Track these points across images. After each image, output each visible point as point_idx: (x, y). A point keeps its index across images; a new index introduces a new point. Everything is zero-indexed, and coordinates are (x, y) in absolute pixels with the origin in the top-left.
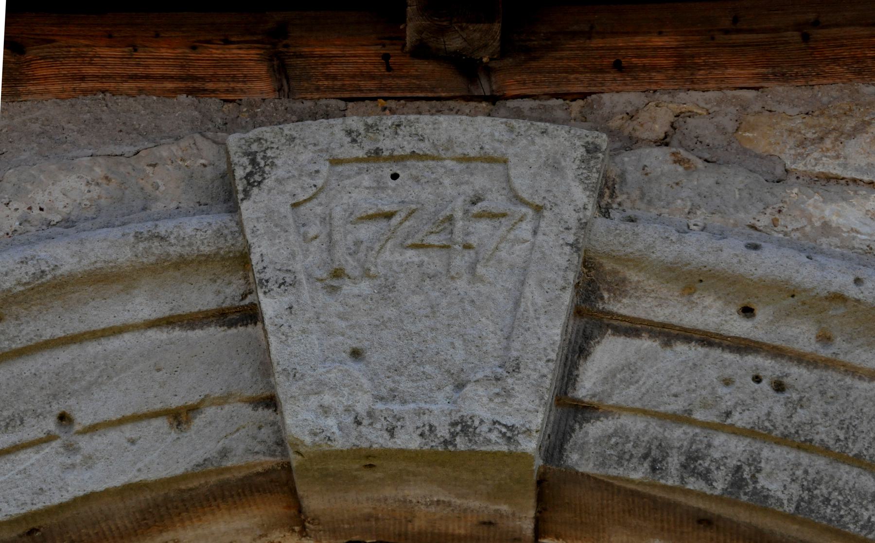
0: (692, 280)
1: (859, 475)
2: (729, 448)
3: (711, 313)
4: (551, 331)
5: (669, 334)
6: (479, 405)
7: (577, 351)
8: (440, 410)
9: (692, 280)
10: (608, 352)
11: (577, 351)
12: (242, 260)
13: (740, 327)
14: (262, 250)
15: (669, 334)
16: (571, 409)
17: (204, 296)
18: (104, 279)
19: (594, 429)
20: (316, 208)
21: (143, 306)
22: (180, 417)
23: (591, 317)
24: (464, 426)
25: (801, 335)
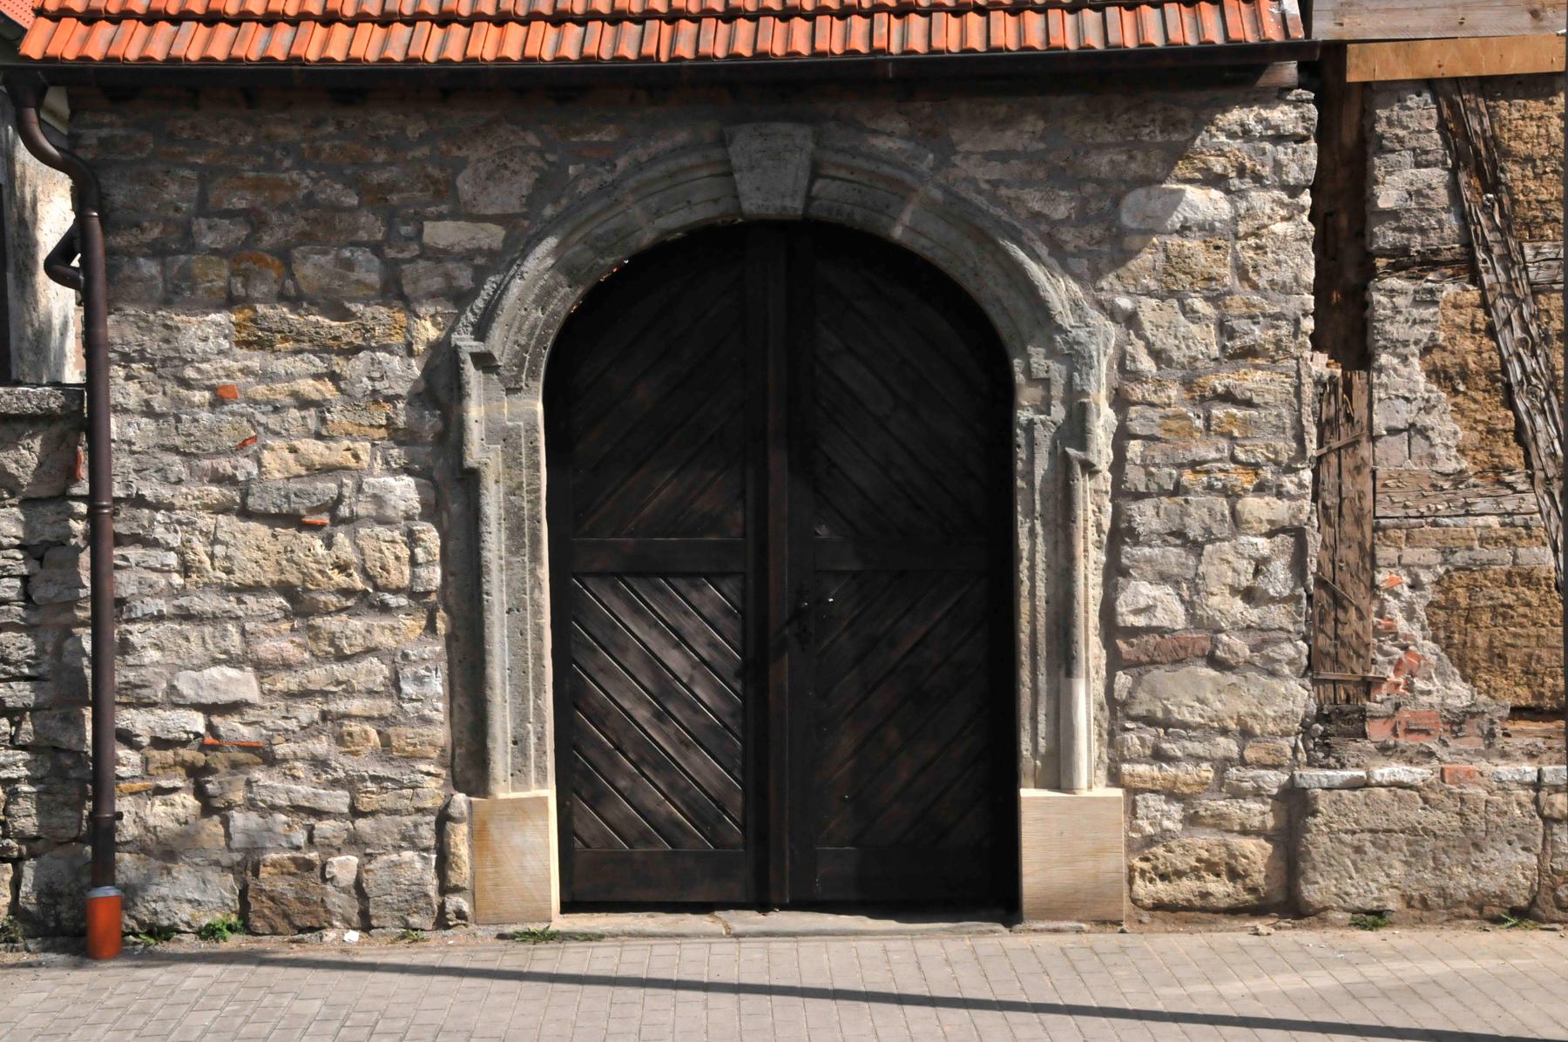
0: (839, 166)
1: (1023, 408)
2: (847, 208)
3: (843, 174)
4: (804, 183)
5: (834, 178)
6: (788, 203)
7: (811, 183)
8: (778, 203)
9: (839, 166)
10: (819, 184)
11: (811, 183)
12: (729, 161)
13: (850, 177)
14: (735, 161)
15: (834, 178)
16: (809, 198)
17: (720, 169)
18: (694, 167)
19: (816, 203)
20: (428, 835)
21: (705, 173)
22: (716, 201)
23: (815, 173)
24: (784, 208)
25: (864, 179)
